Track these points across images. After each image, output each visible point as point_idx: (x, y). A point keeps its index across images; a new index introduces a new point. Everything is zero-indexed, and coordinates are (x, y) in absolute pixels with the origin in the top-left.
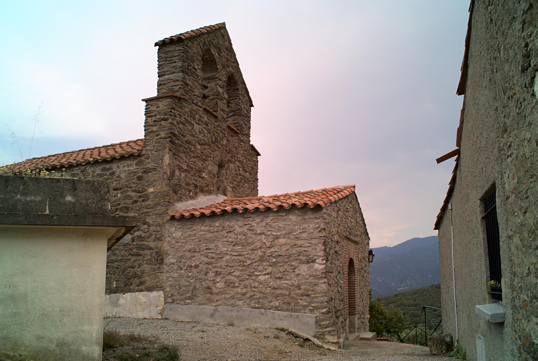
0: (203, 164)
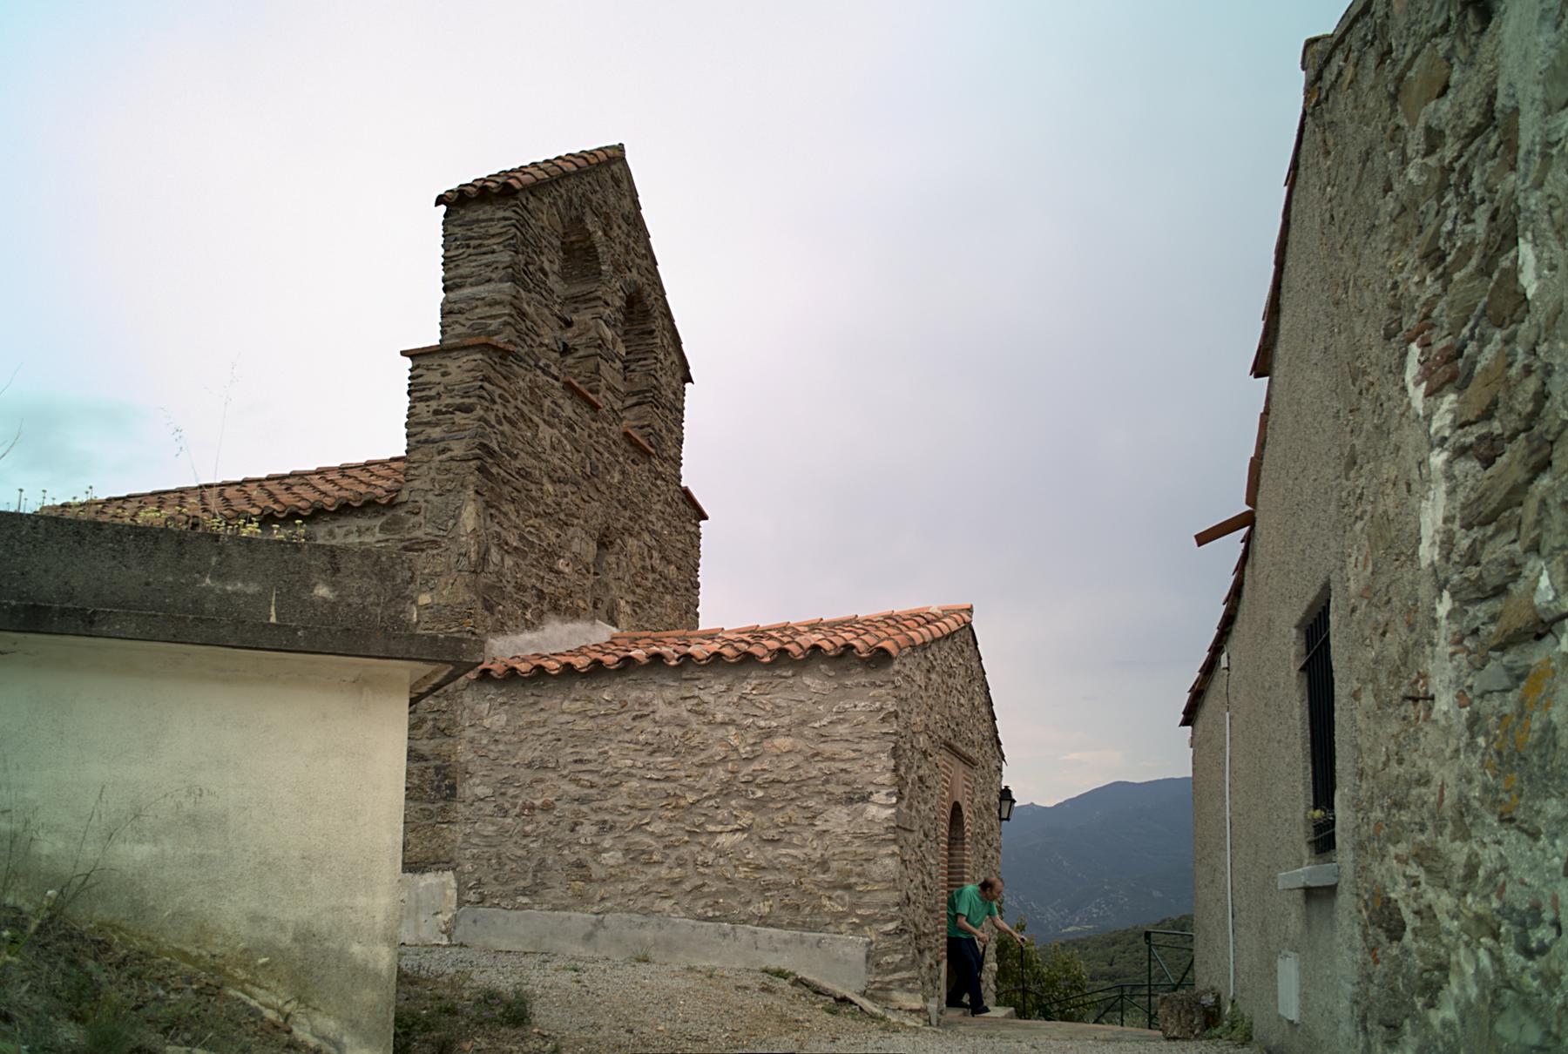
0: (558, 536)
